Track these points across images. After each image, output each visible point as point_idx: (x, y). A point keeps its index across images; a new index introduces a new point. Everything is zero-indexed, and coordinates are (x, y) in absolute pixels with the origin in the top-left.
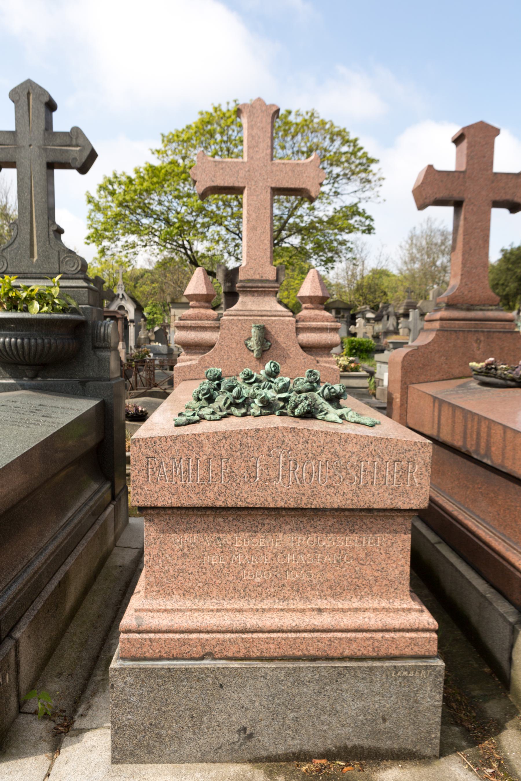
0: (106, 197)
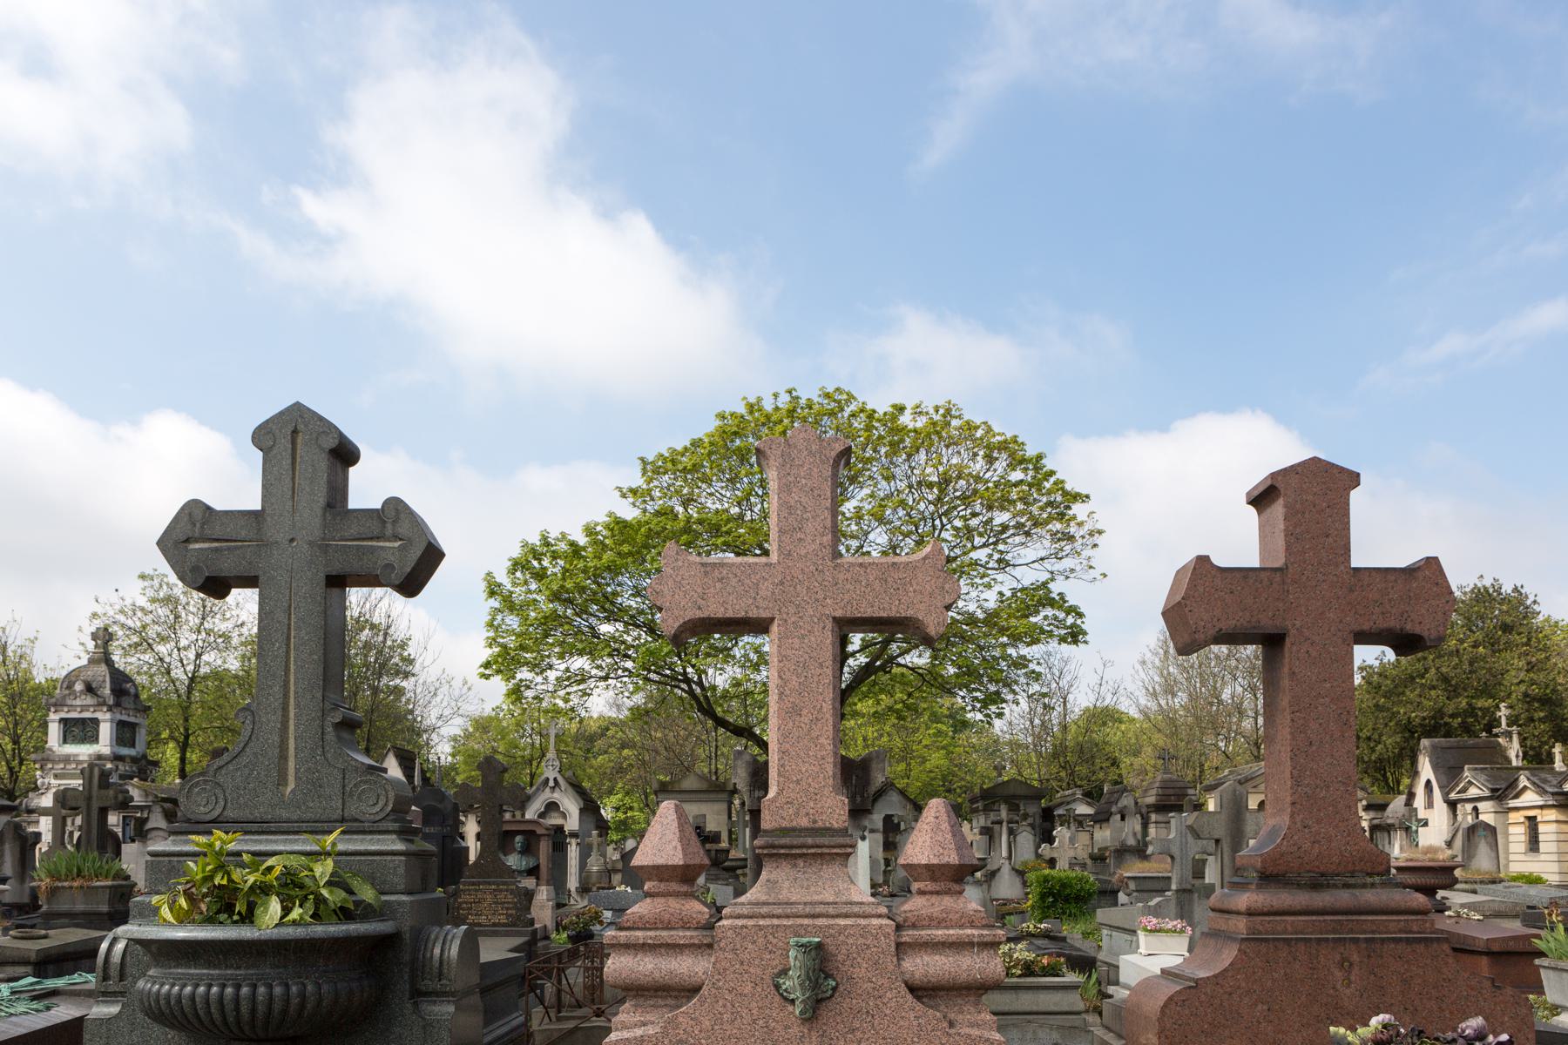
0: (526, 583)
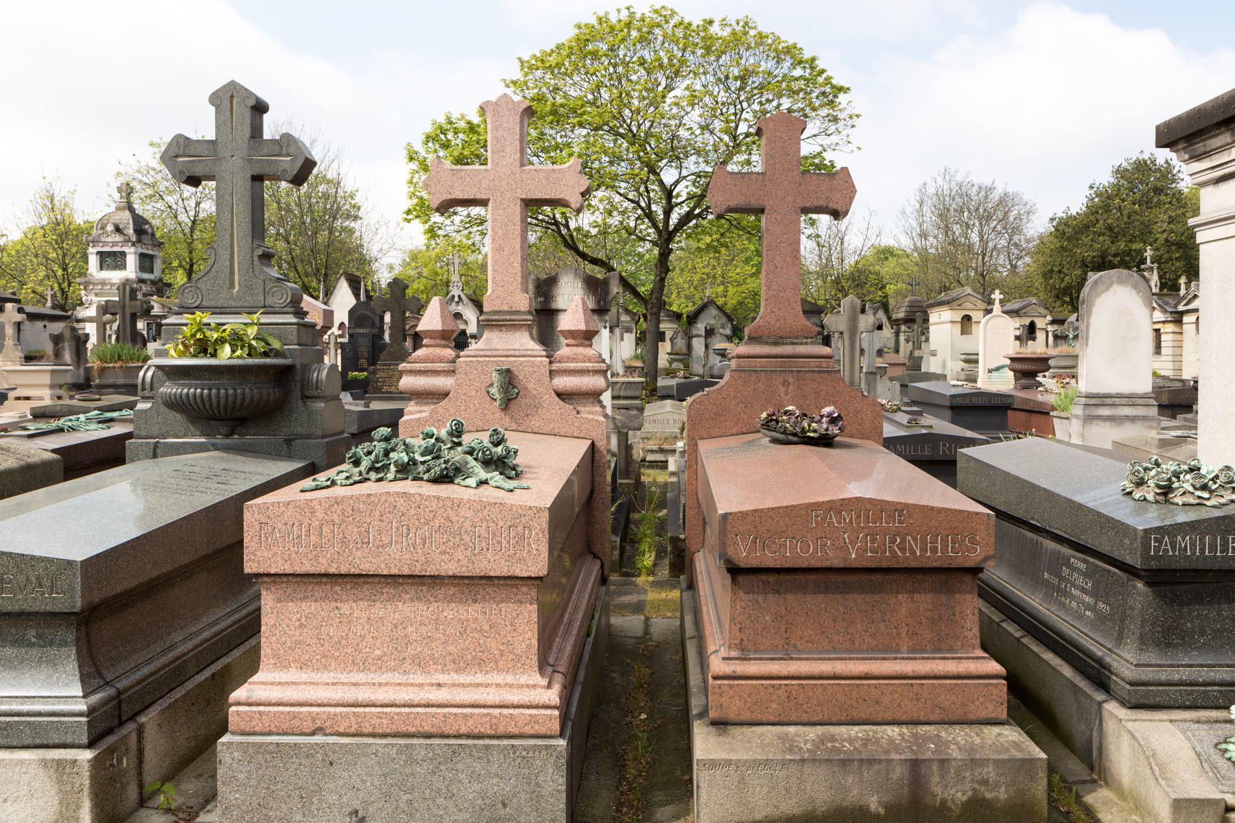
0: (436, 151)
